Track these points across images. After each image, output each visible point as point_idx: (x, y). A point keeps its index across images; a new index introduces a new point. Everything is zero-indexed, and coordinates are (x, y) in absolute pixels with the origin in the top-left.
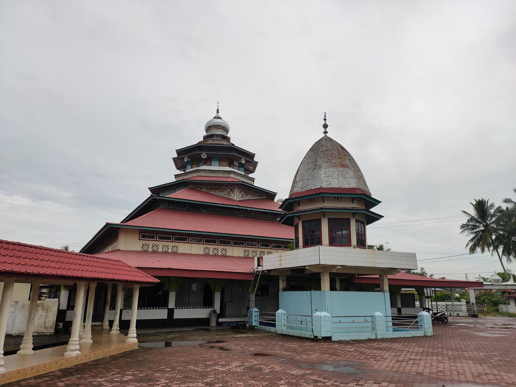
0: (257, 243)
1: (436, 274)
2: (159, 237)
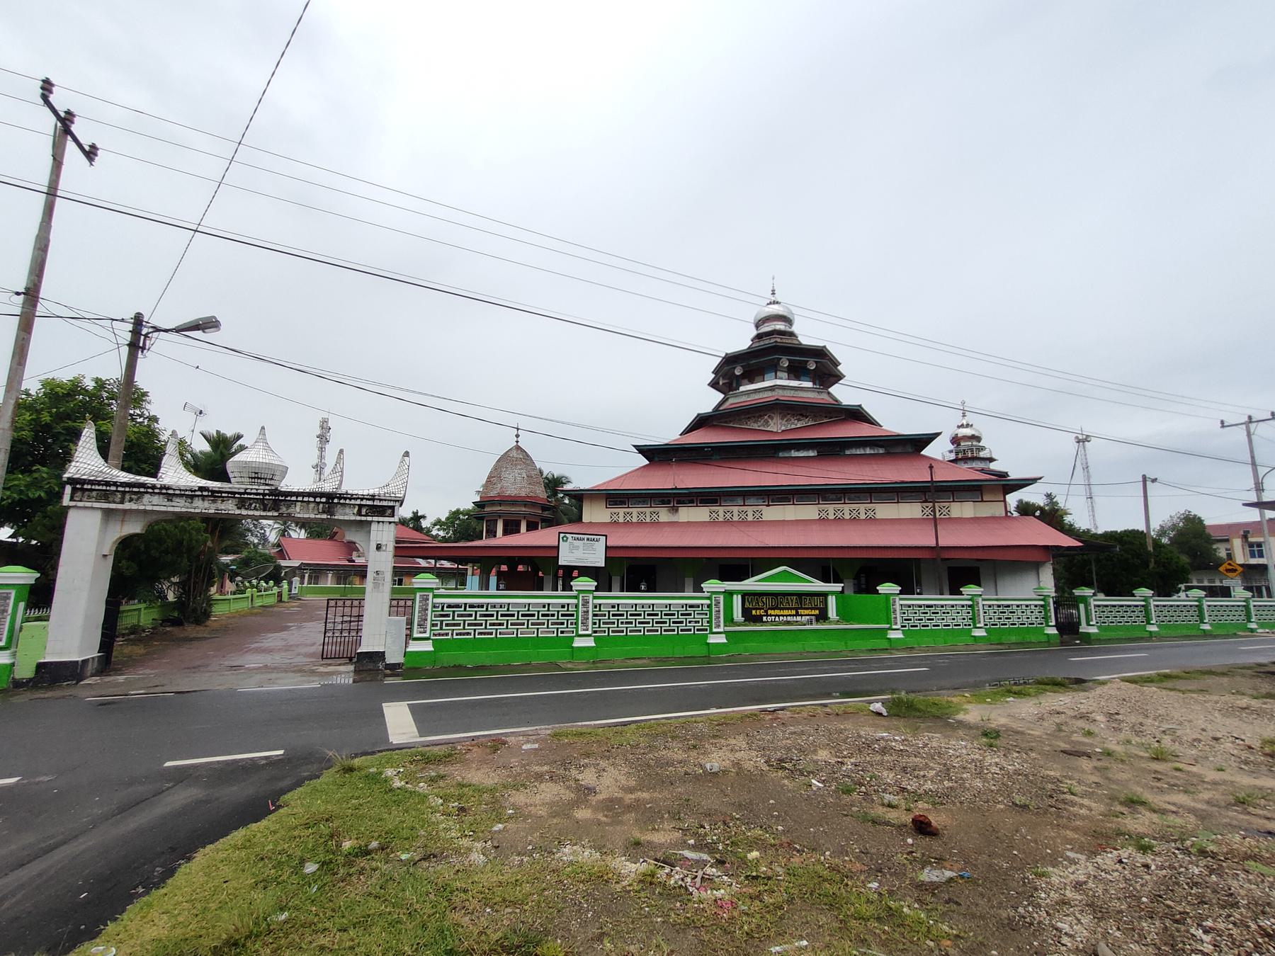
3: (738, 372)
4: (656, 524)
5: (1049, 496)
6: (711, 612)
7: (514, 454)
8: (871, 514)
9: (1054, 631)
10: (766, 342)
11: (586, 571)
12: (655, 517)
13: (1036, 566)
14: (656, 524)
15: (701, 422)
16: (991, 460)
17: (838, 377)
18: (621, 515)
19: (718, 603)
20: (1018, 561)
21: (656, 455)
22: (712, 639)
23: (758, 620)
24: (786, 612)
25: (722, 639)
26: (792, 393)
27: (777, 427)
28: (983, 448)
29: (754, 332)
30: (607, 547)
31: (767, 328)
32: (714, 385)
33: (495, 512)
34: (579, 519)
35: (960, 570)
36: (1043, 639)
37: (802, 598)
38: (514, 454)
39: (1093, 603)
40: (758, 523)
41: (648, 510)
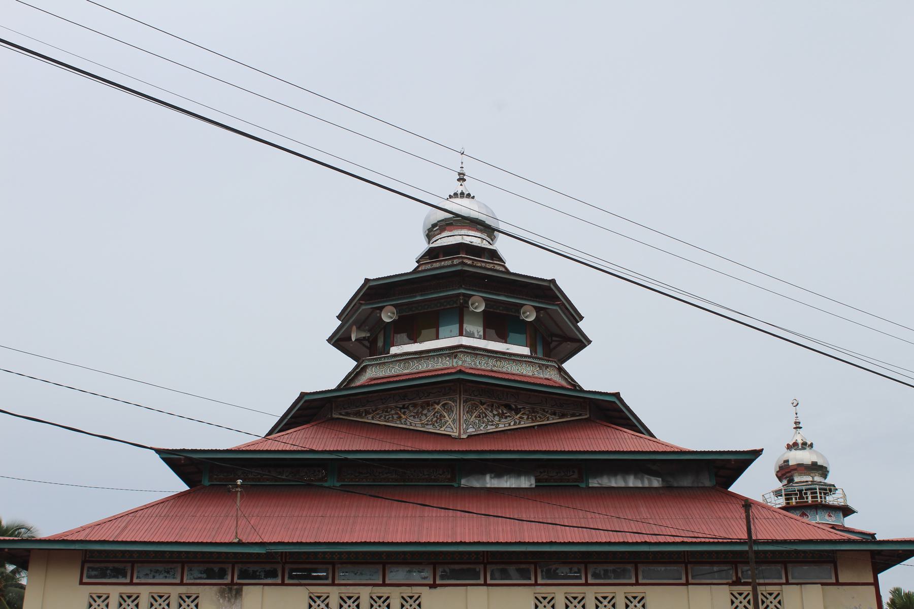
3: (387, 317)
10: (445, 265)
15: (308, 410)
16: (847, 511)
17: (580, 342)
21: (203, 472)
27: (459, 426)
28: (829, 489)
29: (423, 246)
32: (339, 341)
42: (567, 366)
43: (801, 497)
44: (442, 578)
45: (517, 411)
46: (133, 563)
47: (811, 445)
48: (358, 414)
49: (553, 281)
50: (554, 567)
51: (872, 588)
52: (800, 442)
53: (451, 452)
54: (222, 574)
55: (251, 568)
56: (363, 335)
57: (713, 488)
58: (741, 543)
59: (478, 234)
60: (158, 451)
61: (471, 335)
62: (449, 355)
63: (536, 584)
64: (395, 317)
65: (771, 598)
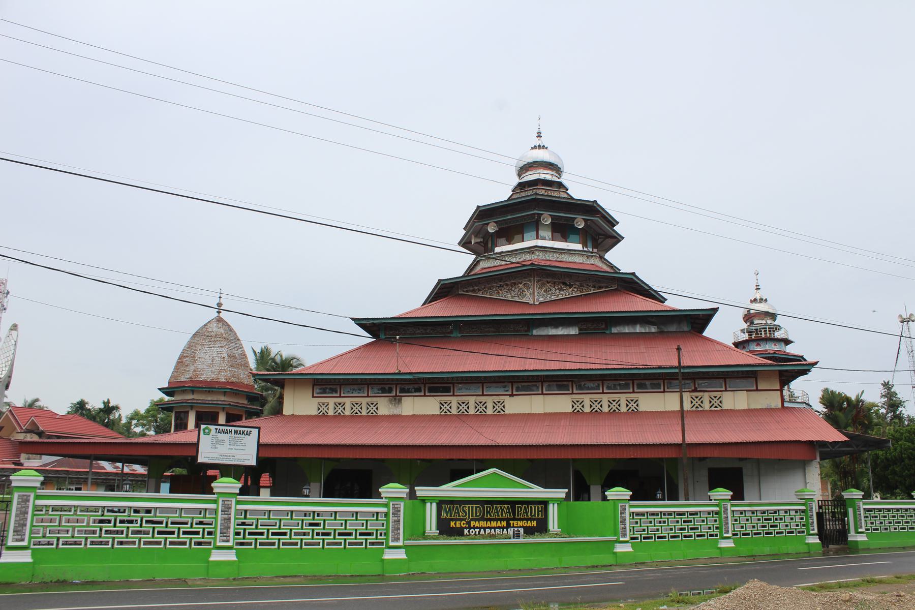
0: (661, 382)
1: (807, 556)
2: (638, 385)
3: (491, 229)
4: (373, 418)
5: (886, 385)
6: (387, 521)
7: (214, 328)
8: (633, 406)
9: (815, 540)
10: (528, 193)
11: (227, 470)
12: (372, 409)
13: (803, 465)
14: (373, 418)
15: (444, 290)
16: (787, 342)
17: (617, 239)
18: (331, 406)
19: (396, 512)
20: (787, 457)
21: (381, 331)
22: (389, 555)
23: (459, 532)
24: (494, 524)
25: (401, 555)
26: (555, 257)
27: (534, 298)
28: (778, 328)
29: (516, 181)
30: (260, 446)
31: (530, 176)
32: (465, 243)
33: (186, 401)
34: (278, 411)
35: (731, 470)
36: (802, 549)
37: (514, 508)
38: (214, 328)
39: (862, 507)
40: (501, 417)
41: (364, 401)
42: (608, 256)
43: (757, 334)
44: (517, 391)
45: (571, 286)
46: (341, 385)
47: (766, 300)
48: (474, 291)
49: (595, 202)
50: (583, 384)
51: (779, 393)
52: (758, 298)
53: (525, 314)
54: (390, 391)
55: (407, 387)
56: (478, 240)
57: (689, 332)
58: (675, 368)
59: (550, 172)
60: (353, 319)
61: (544, 238)
62: (529, 252)
63: (573, 393)
64: (496, 229)
65: (715, 400)
